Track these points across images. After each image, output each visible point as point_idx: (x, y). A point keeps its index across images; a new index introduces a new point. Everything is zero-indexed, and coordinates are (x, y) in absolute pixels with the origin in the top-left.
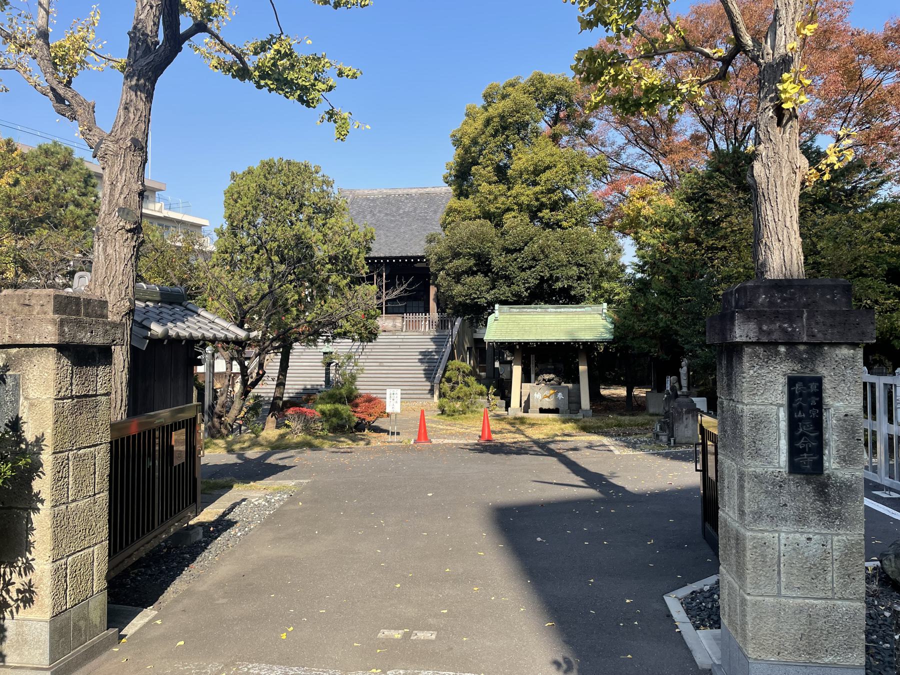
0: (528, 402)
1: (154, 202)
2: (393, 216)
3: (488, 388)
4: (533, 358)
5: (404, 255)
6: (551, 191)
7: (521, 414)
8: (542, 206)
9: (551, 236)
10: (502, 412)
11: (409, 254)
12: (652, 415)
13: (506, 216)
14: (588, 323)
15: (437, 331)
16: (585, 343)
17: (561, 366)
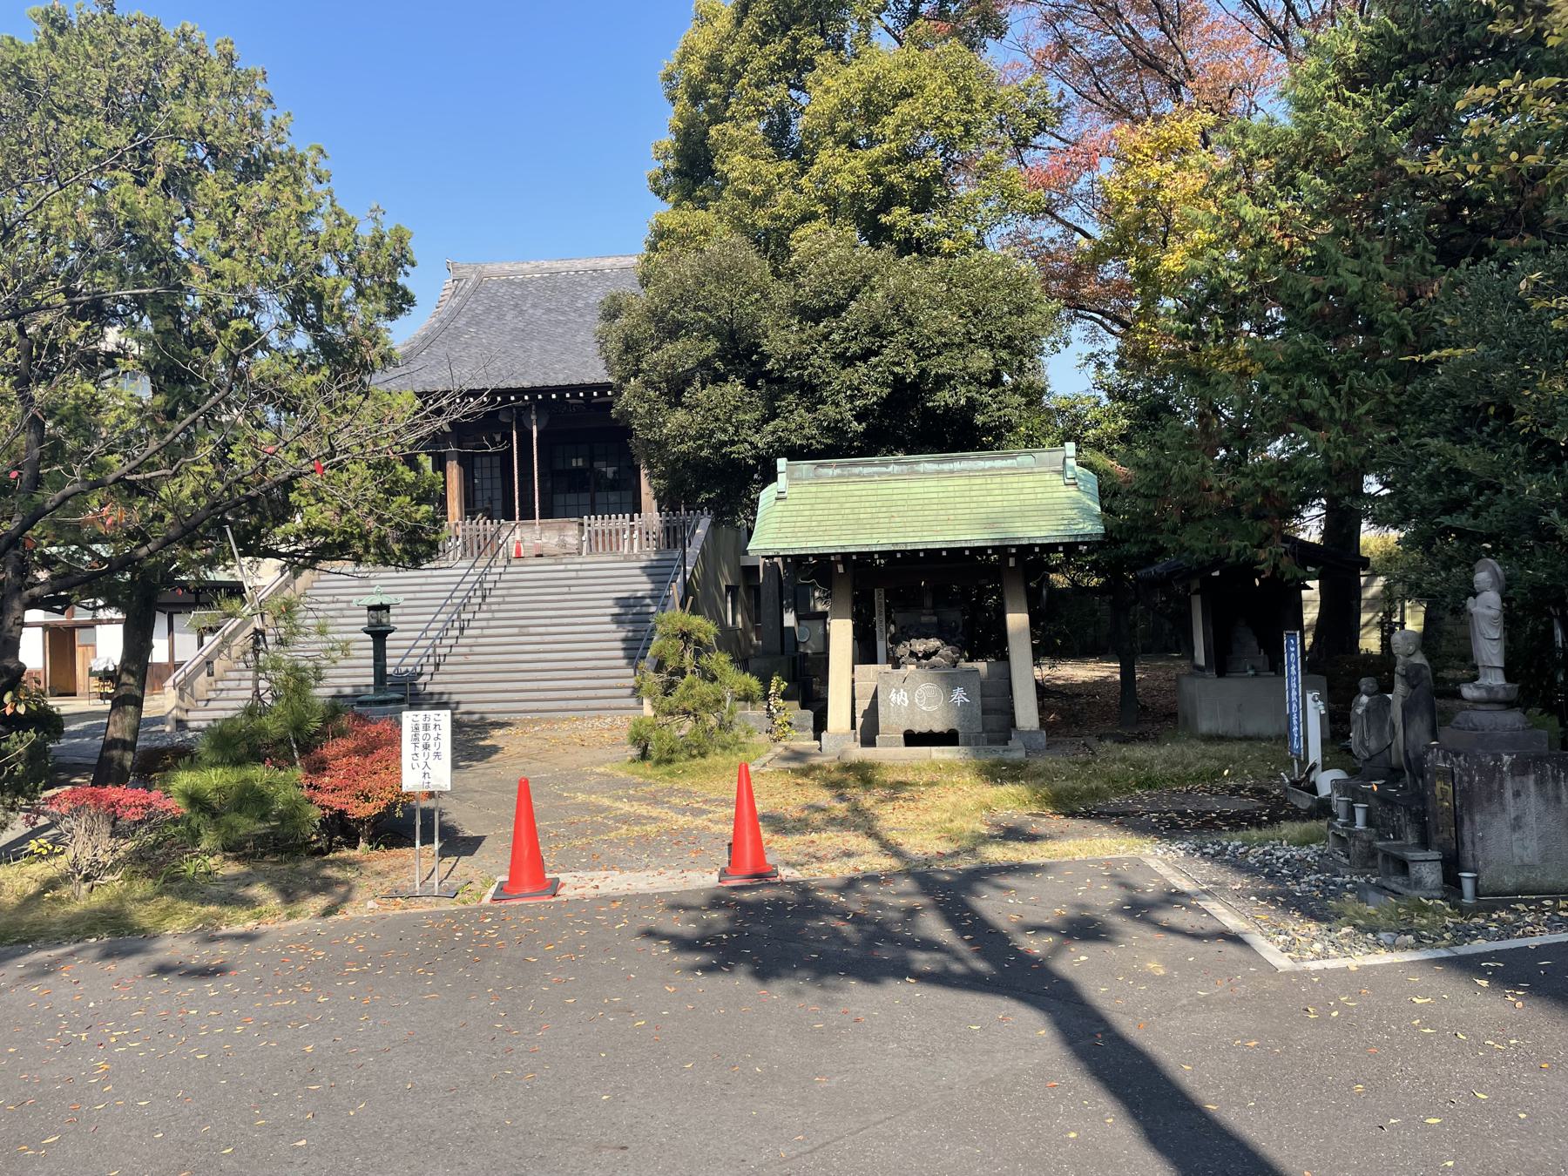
0: (872, 713)
2: (564, 313)
3: (765, 681)
4: (879, 598)
5: (575, 382)
6: (906, 156)
7: (858, 753)
8: (890, 198)
9: (914, 275)
10: (805, 742)
11: (587, 380)
12: (1211, 738)
13: (801, 232)
14: (1027, 497)
15: (656, 553)
16: (1025, 550)
17: (955, 617)
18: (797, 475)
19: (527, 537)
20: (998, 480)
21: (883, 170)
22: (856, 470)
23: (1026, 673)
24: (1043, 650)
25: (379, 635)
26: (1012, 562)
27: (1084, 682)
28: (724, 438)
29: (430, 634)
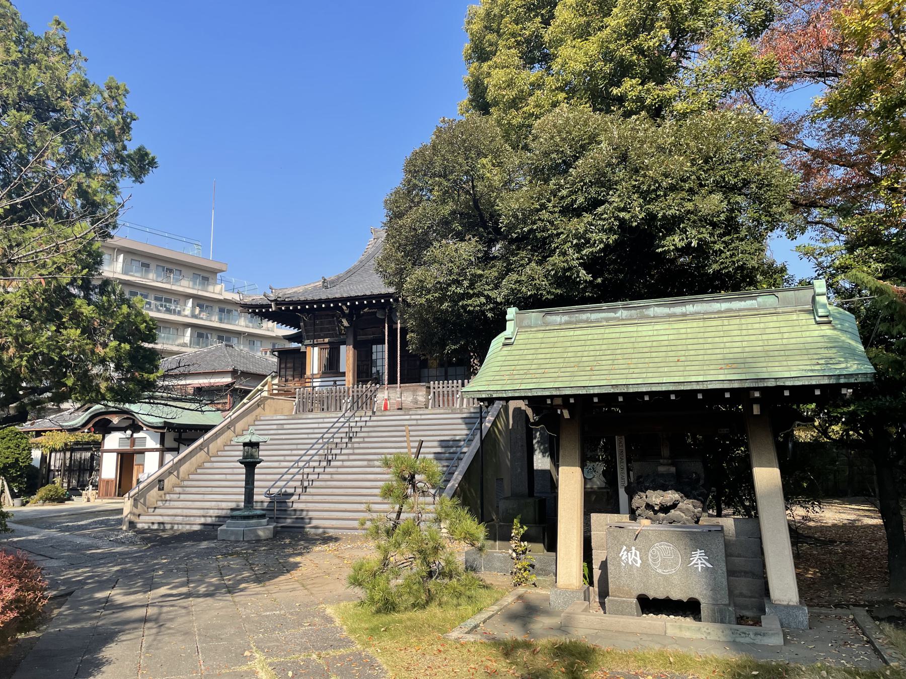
1: (215, 284)
17: (695, 467)
18: (525, 323)
19: (392, 395)
20: (737, 321)
21: (612, 46)
22: (584, 316)
23: (776, 519)
24: (793, 491)
25: (250, 464)
26: (756, 410)
27: (834, 525)
28: (459, 290)
29: (312, 464)
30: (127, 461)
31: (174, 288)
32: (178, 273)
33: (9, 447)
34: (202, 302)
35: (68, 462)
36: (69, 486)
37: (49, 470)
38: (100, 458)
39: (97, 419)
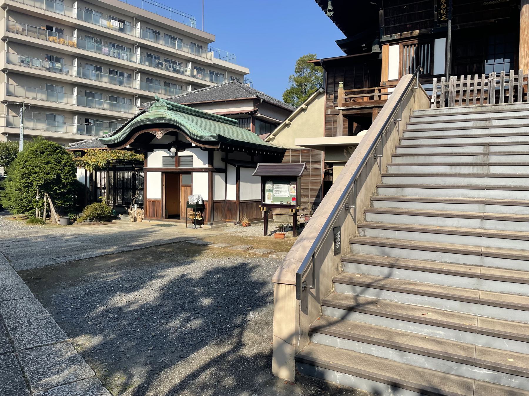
1: (207, 51)
30: (173, 180)
31: (178, 52)
32: (180, 41)
33: (48, 163)
34: (198, 65)
35: (112, 181)
36: (115, 203)
37: (97, 188)
38: (145, 178)
39: (138, 134)
